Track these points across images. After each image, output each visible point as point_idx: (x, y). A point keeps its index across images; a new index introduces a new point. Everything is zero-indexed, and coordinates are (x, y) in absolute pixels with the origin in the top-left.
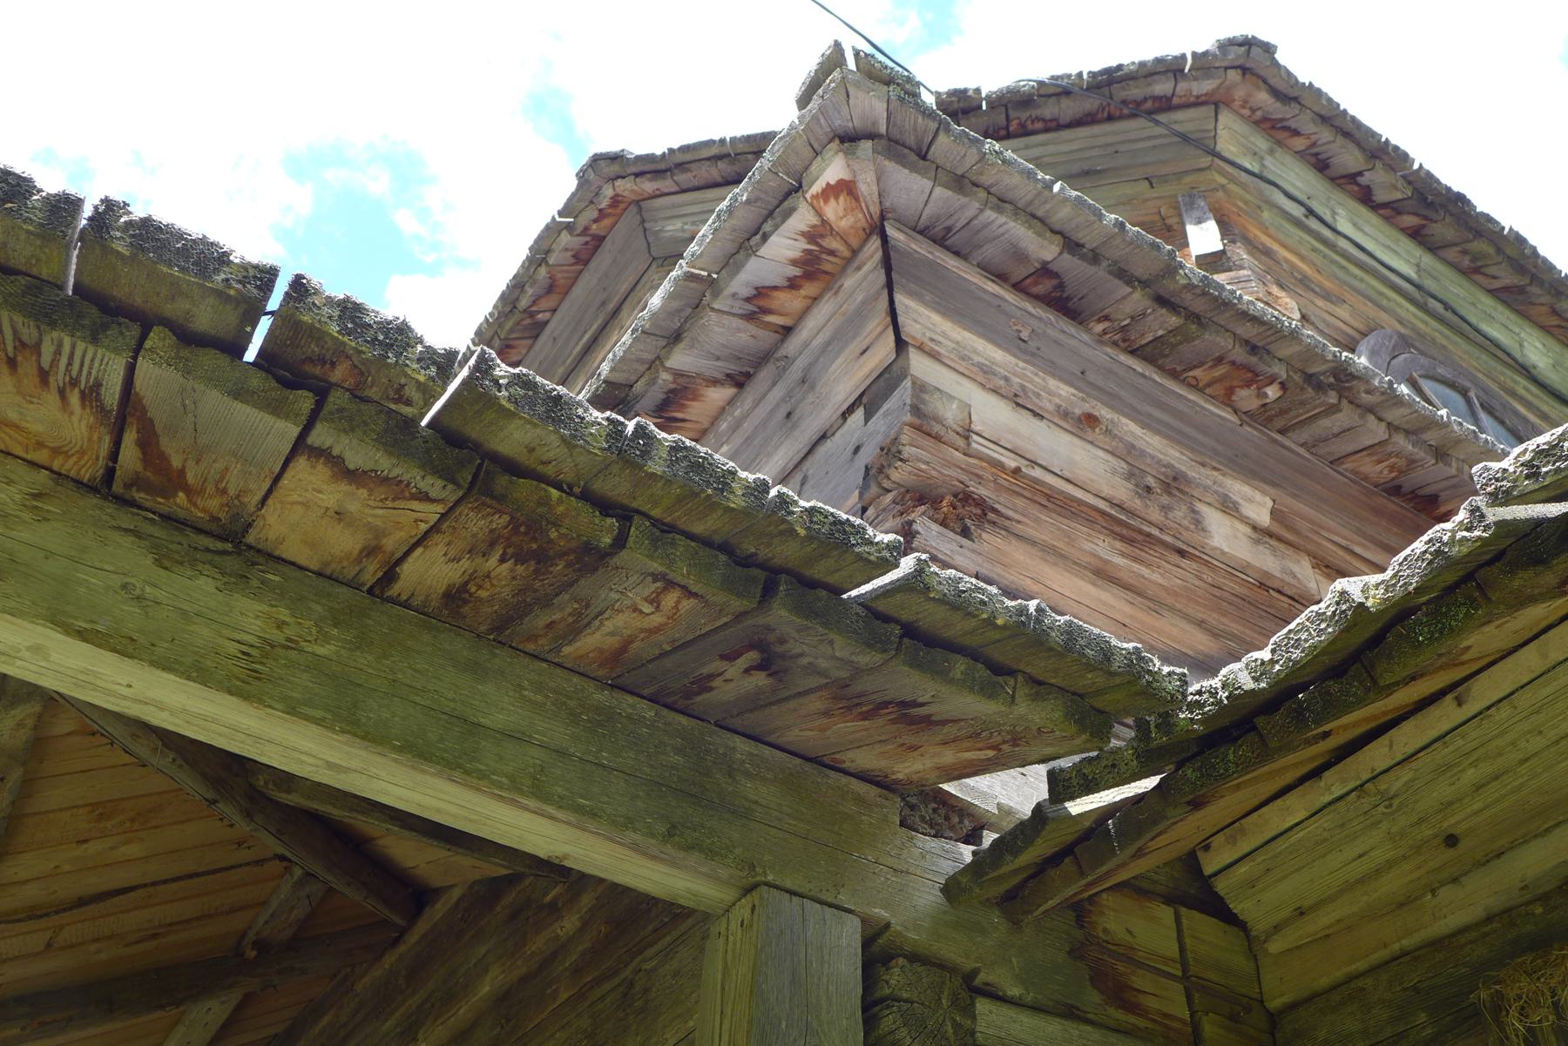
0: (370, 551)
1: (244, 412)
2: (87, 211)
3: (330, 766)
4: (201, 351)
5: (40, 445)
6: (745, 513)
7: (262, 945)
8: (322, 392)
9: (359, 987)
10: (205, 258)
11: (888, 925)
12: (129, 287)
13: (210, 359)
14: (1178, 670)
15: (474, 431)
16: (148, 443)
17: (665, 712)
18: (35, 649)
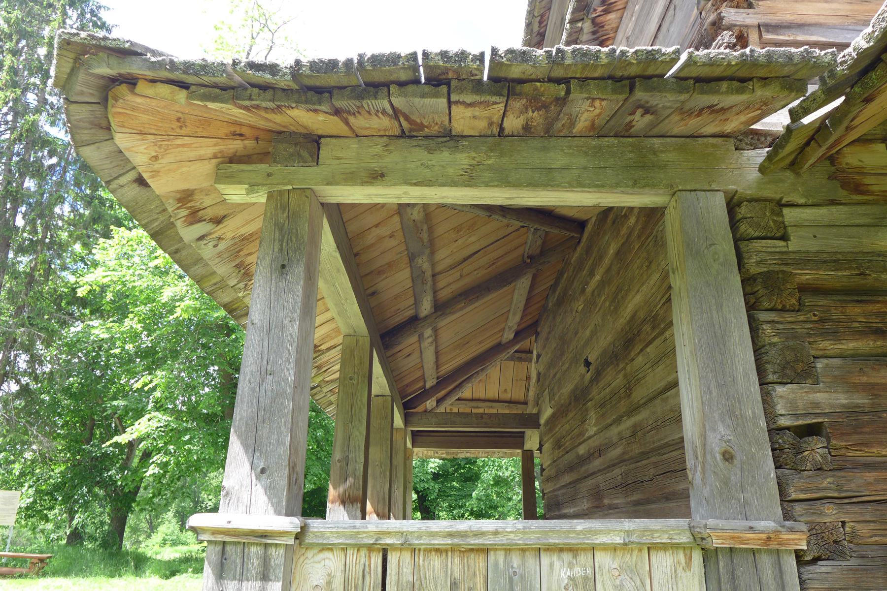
0: (491, 124)
1: (427, 101)
2: (356, 61)
3: (507, 198)
4: (407, 87)
5: (379, 130)
6: (609, 64)
7: (531, 257)
8: (448, 84)
9: (572, 262)
10: (394, 59)
11: (737, 191)
12: (378, 77)
13: (411, 88)
14: (830, 50)
15: (502, 74)
16: (407, 118)
17: (622, 139)
18: (405, 193)
